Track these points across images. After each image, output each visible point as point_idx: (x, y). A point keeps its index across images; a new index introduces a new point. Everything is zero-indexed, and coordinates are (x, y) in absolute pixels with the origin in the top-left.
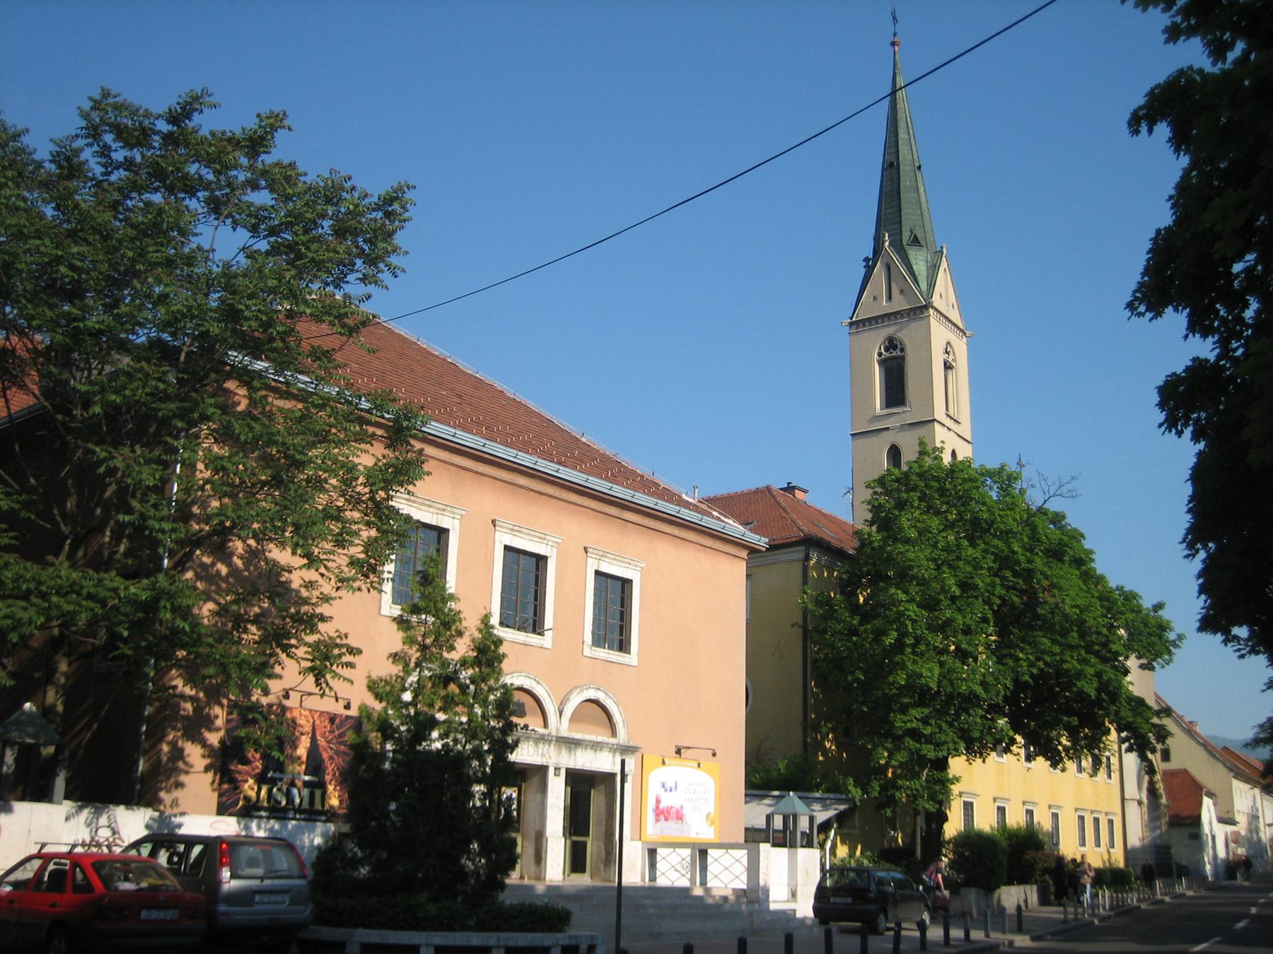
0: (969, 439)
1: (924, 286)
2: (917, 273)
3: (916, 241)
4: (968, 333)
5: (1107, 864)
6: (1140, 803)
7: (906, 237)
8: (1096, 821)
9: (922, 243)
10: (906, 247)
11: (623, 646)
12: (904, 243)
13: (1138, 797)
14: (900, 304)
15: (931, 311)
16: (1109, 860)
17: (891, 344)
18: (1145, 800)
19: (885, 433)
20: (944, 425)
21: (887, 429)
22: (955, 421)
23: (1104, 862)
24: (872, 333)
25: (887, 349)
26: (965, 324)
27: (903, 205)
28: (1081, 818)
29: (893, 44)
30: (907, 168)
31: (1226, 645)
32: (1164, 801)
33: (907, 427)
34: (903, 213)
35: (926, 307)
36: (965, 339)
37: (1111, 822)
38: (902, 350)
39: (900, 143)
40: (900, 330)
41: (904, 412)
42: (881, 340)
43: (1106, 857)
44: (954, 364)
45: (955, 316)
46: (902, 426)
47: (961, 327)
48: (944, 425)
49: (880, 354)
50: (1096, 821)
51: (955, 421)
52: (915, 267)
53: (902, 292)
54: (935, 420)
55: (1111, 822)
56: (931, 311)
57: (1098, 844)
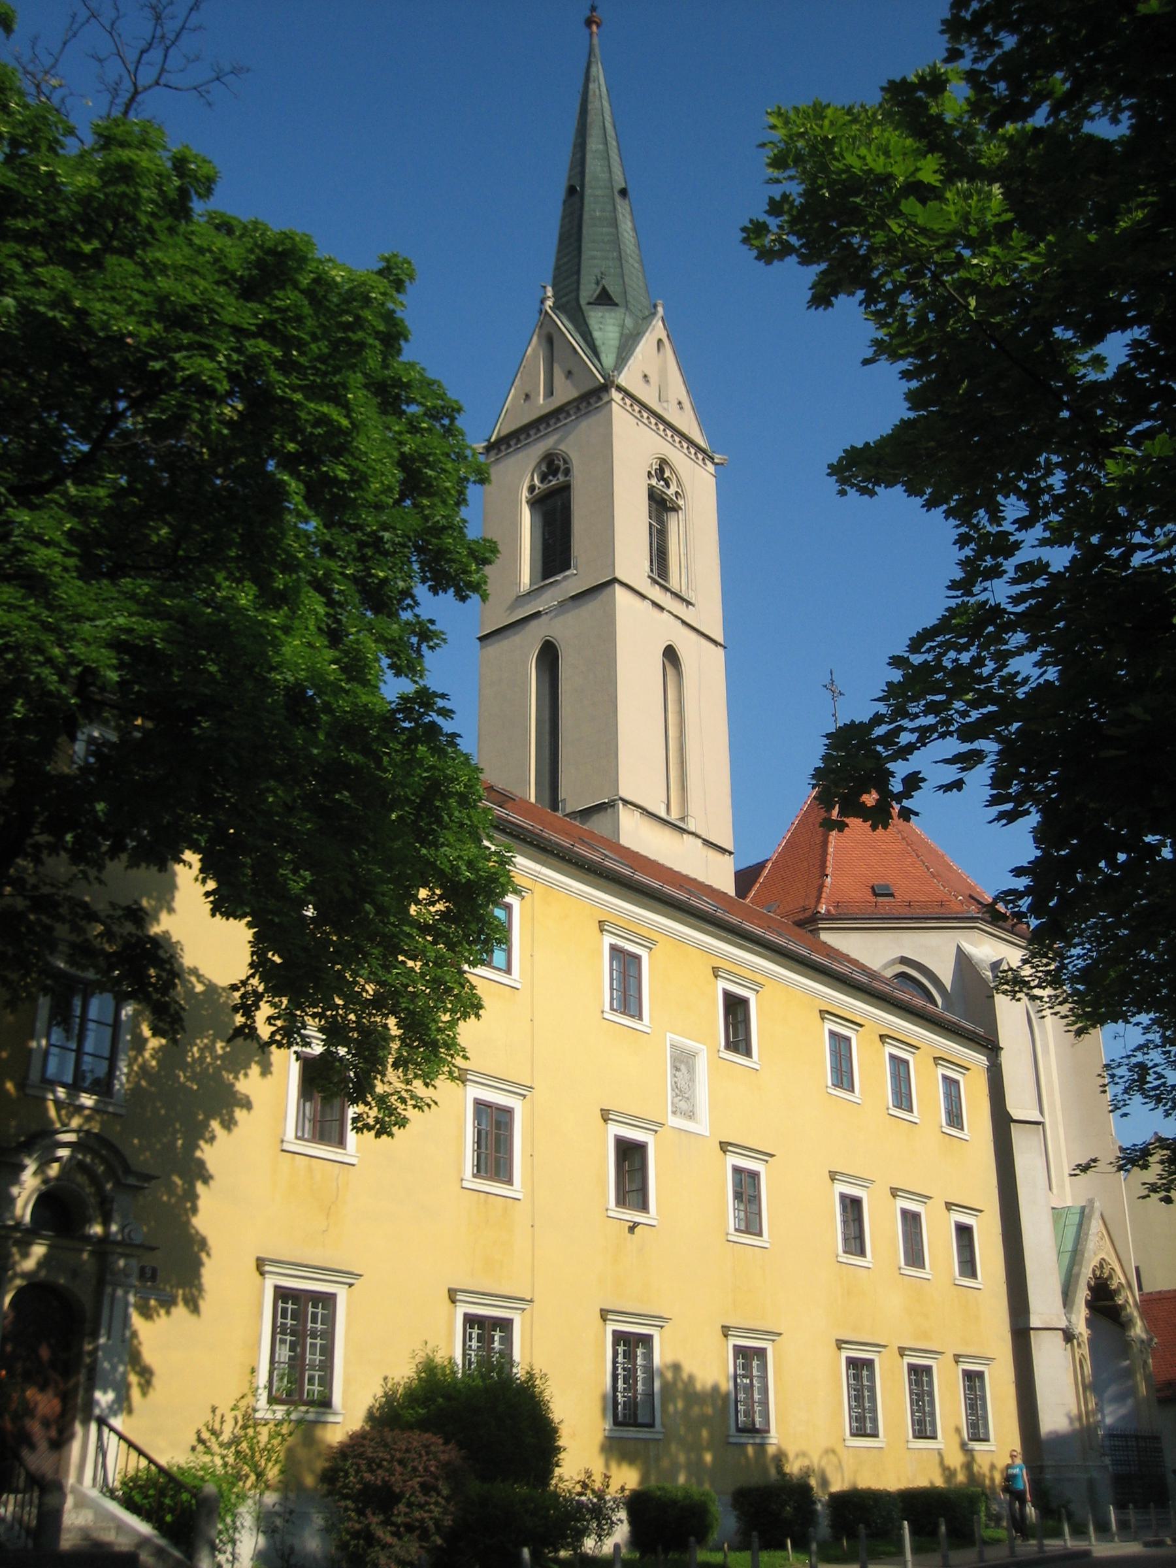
0: (720, 639)
1: (609, 359)
2: (598, 343)
3: (605, 299)
4: (718, 458)
5: (961, 1477)
6: (1069, 1336)
7: (588, 291)
8: (920, 1375)
9: (616, 300)
10: (584, 307)
11: (862, 1253)
12: (583, 302)
13: (1063, 1324)
14: (566, 392)
15: (616, 395)
16: (968, 1466)
17: (552, 465)
18: (1081, 1328)
19: (534, 624)
20: (643, 597)
21: (537, 615)
22: (682, 599)
23: (948, 1473)
24: (521, 455)
25: (543, 479)
26: (710, 441)
27: (586, 245)
28: (860, 1368)
29: (589, 22)
30: (599, 192)
31: (946, 518)
32: (1138, 1330)
33: (570, 603)
34: (584, 257)
35: (605, 388)
36: (710, 467)
37: (973, 1379)
38: (567, 472)
39: (589, 156)
40: (559, 441)
41: (565, 578)
42: (532, 464)
43: (956, 1460)
44: (681, 502)
45: (687, 422)
46: (562, 604)
47: (702, 443)
48: (643, 597)
49: (532, 488)
50: (920, 1375)
51: (682, 599)
52: (596, 334)
53: (569, 374)
54: (615, 580)
55: (973, 1379)
56: (616, 395)
57: (924, 1428)
